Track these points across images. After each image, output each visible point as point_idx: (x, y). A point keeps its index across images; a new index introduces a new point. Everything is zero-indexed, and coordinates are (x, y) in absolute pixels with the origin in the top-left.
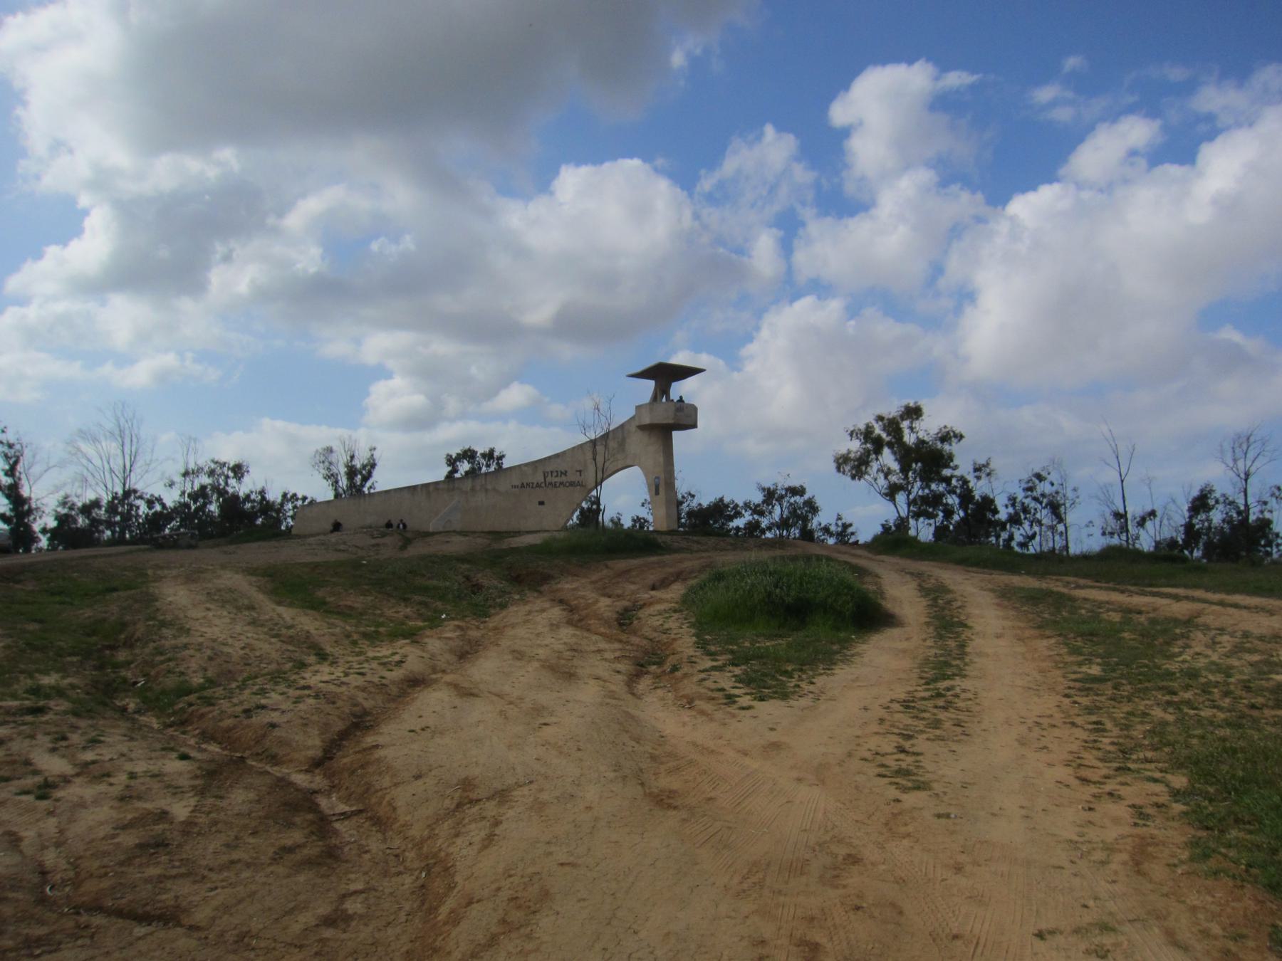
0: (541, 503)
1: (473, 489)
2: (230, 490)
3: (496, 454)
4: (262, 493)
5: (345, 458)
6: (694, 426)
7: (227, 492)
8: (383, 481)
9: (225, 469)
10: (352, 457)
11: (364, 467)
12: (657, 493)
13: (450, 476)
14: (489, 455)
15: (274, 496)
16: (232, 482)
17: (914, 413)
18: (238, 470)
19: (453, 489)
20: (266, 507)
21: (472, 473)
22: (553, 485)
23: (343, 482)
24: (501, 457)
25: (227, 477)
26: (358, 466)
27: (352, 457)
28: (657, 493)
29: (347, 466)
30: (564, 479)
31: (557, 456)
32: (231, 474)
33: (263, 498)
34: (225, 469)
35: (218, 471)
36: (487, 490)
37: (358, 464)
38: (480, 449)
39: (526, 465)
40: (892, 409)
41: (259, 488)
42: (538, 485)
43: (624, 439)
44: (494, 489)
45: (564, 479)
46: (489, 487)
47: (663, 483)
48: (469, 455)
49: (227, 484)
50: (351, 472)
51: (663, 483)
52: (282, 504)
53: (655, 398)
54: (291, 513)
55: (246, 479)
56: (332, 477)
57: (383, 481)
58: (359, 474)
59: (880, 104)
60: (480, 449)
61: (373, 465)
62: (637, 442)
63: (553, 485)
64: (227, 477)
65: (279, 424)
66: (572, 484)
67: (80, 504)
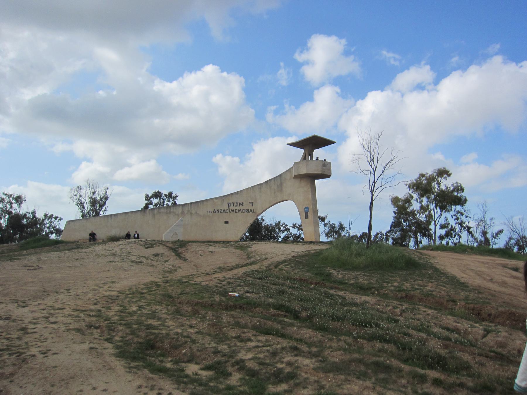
0: (227, 222)
1: (183, 213)
2: (14, 211)
3: (173, 195)
4: (34, 213)
5: (90, 193)
6: (328, 176)
7: (11, 212)
8: (110, 209)
9: (11, 198)
10: (94, 193)
11: (101, 199)
12: (307, 217)
13: (146, 207)
14: (170, 195)
15: (40, 215)
16: (15, 206)
17: (443, 173)
18: (19, 200)
19: (170, 213)
20: (34, 222)
21: (160, 205)
22: (235, 211)
23: (88, 207)
24: (176, 197)
25: (11, 203)
26: (98, 198)
27: (94, 193)
28: (307, 217)
29: (90, 198)
30: (241, 207)
31: (237, 193)
32: (14, 201)
33: (34, 216)
34: (11, 198)
35: (7, 199)
36: (191, 213)
37: (97, 197)
38: (165, 192)
39: (217, 198)
40: (430, 171)
41: (31, 210)
42: (225, 211)
43: (281, 184)
44: (196, 213)
45: (241, 207)
46: (193, 212)
47: (309, 211)
48: (157, 195)
49: (11, 207)
50: (94, 202)
51: (309, 211)
52: (43, 220)
53: (304, 158)
54: (48, 225)
55: (23, 205)
56: (81, 205)
57: (110, 209)
58: (97, 204)
59: (323, 53)
60: (165, 192)
61: (107, 198)
62: (291, 186)
63: (235, 211)
64: (11, 203)
65: (36, 184)
66: (247, 211)
67: (57, 227)
